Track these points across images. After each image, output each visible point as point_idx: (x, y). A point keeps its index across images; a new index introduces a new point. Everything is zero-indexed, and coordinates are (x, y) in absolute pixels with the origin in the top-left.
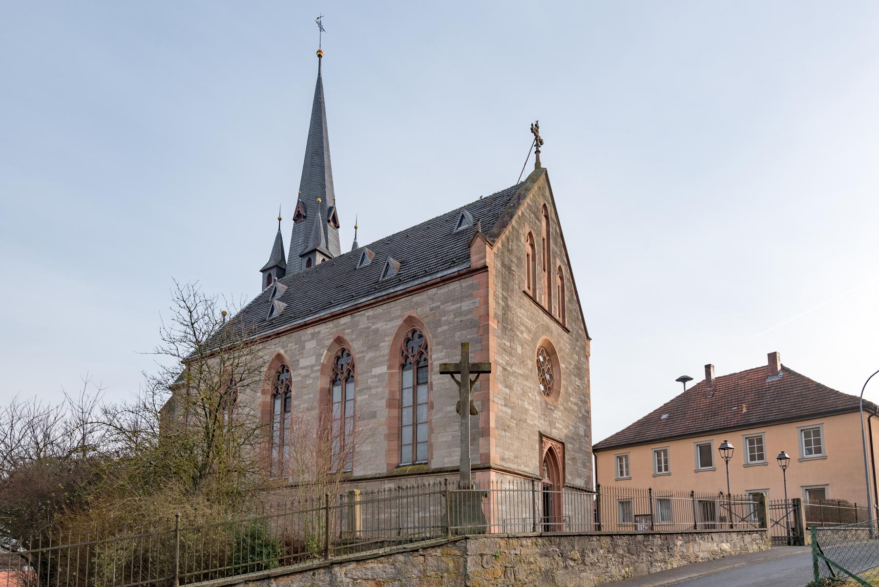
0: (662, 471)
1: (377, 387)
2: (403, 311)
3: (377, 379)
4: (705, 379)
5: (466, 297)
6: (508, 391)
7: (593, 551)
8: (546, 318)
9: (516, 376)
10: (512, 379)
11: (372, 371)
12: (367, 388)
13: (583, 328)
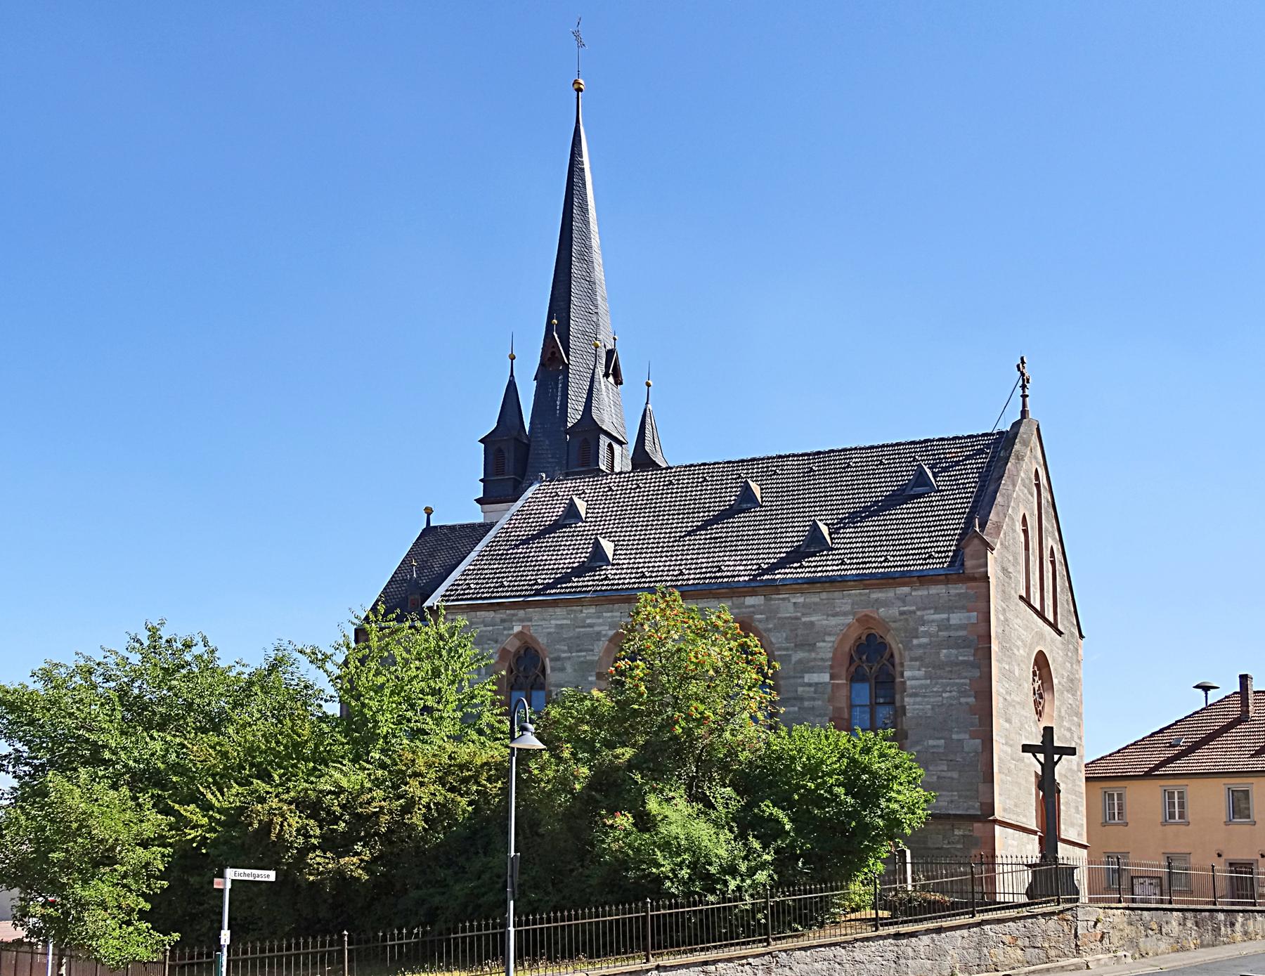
0: (1175, 818)
1: (814, 699)
2: (856, 607)
3: (813, 689)
4: (1238, 690)
5: (956, 608)
6: (1007, 725)
7: (1167, 923)
8: (1040, 621)
9: (1014, 706)
10: (1011, 709)
11: (804, 677)
12: (795, 699)
13: (1075, 623)
